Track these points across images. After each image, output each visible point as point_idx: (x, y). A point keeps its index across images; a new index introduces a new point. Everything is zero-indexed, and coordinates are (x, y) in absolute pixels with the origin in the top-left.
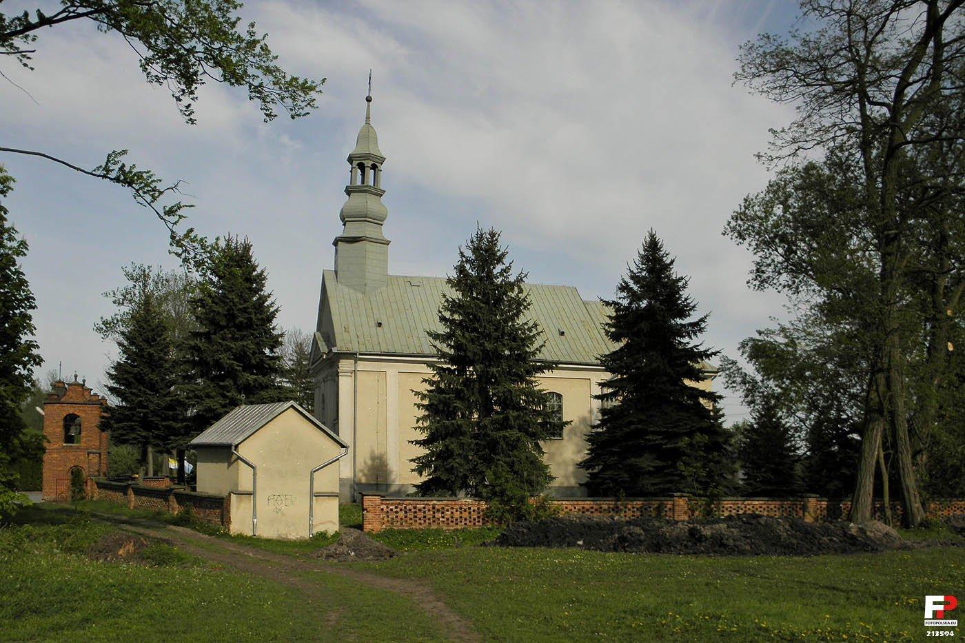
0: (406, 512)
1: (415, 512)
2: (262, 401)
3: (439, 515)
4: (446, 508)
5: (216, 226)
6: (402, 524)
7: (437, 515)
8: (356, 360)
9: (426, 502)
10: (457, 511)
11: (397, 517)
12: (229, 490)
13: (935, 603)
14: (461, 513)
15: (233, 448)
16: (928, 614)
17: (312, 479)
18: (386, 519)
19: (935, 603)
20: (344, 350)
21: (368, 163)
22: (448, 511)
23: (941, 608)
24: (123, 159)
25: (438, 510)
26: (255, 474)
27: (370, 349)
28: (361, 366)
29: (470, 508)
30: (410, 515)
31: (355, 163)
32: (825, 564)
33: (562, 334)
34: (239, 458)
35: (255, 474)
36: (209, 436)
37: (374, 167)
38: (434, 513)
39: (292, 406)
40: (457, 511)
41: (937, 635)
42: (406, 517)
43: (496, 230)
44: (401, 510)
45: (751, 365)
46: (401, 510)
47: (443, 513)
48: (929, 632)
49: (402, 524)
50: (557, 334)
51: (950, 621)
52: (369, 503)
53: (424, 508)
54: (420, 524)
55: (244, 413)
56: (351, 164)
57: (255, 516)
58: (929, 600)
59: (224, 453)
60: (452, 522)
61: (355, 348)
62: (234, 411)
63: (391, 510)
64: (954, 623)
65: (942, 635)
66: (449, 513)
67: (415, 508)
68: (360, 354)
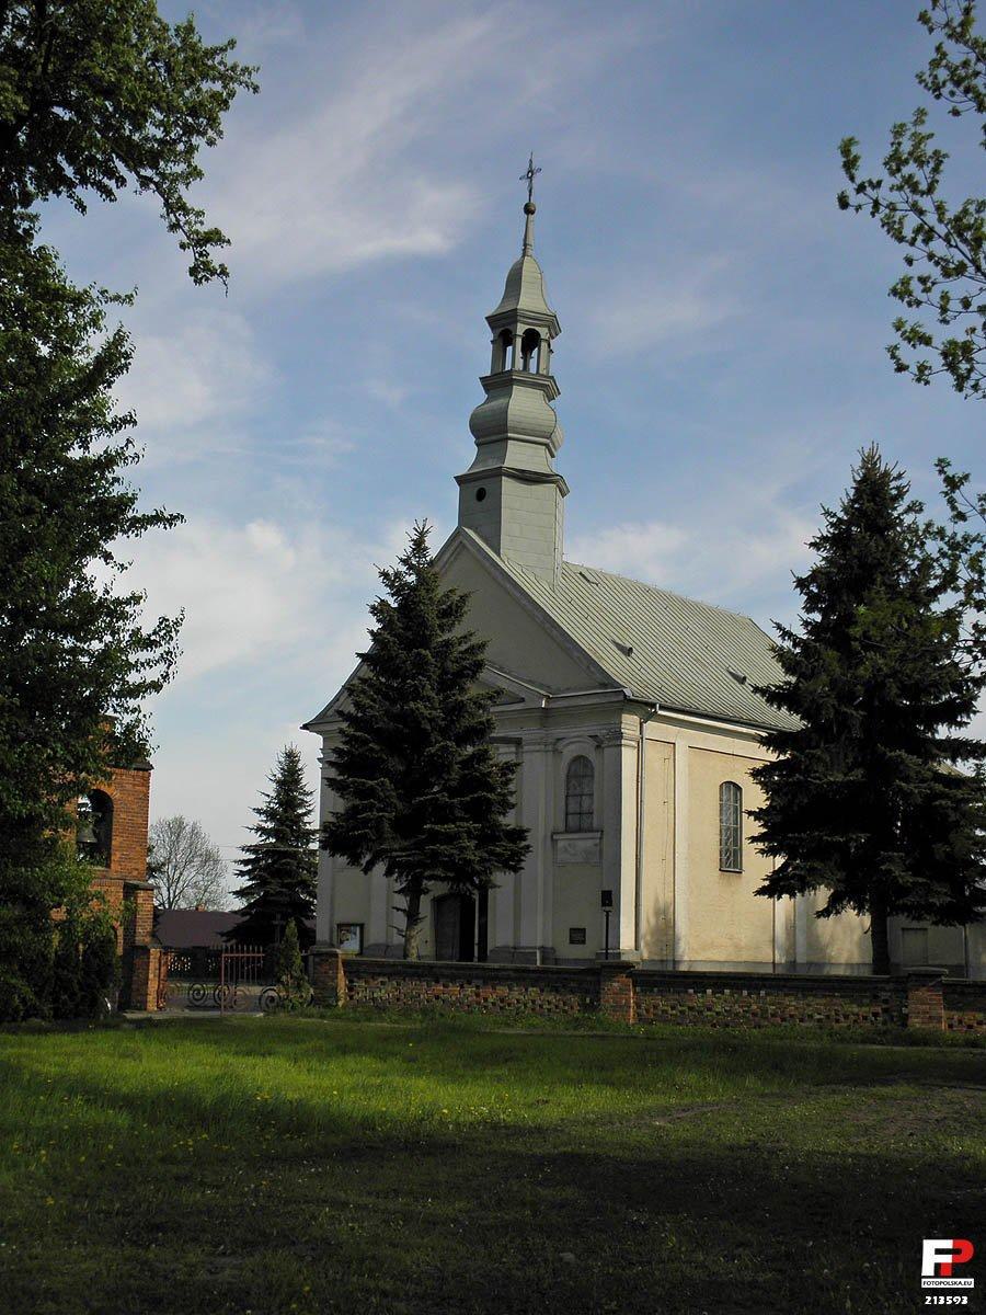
5: (858, 919)
8: (652, 716)
13: (939, 1252)
16: (928, 1269)
19: (939, 1252)
23: (947, 1259)
24: (856, 468)
28: (652, 728)
32: (122, 775)
41: (942, 1302)
45: (504, 761)
48: (929, 1298)
51: (963, 1280)
58: (929, 1246)
64: (969, 1283)
65: (950, 1302)
68: (662, 708)
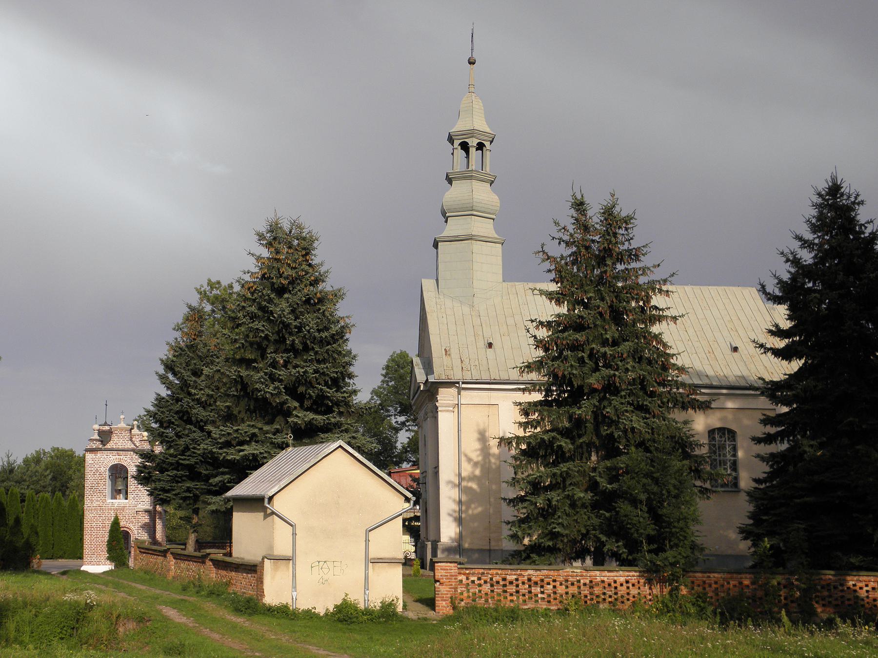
0: (492, 585)
1: (505, 586)
2: (316, 443)
3: (536, 590)
4: (546, 580)
6: (487, 601)
7: (533, 590)
9: (519, 572)
10: (561, 584)
11: (480, 591)
12: (264, 553)
14: (567, 587)
15: (266, 500)
17: (367, 541)
18: (465, 594)
20: (443, 379)
21: (473, 142)
22: (548, 584)
25: (536, 583)
26: (294, 534)
27: (476, 376)
28: (467, 397)
29: (579, 581)
30: (498, 589)
31: (457, 143)
33: (735, 349)
34: (273, 513)
35: (294, 534)
36: (242, 489)
37: (480, 146)
38: (530, 586)
39: (340, 446)
40: (561, 584)
42: (492, 591)
43: (623, 210)
44: (486, 582)
46: (486, 582)
47: (542, 587)
49: (487, 601)
50: (728, 351)
52: (443, 573)
53: (517, 580)
54: (512, 601)
55: (293, 456)
56: (453, 144)
57: (294, 587)
59: (256, 503)
60: (555, 599)
61: (457, 376)
62: (279, 455)
63: (473, 582)
66: (551, 587)
67: (504, 579)
68: (463, 383)
